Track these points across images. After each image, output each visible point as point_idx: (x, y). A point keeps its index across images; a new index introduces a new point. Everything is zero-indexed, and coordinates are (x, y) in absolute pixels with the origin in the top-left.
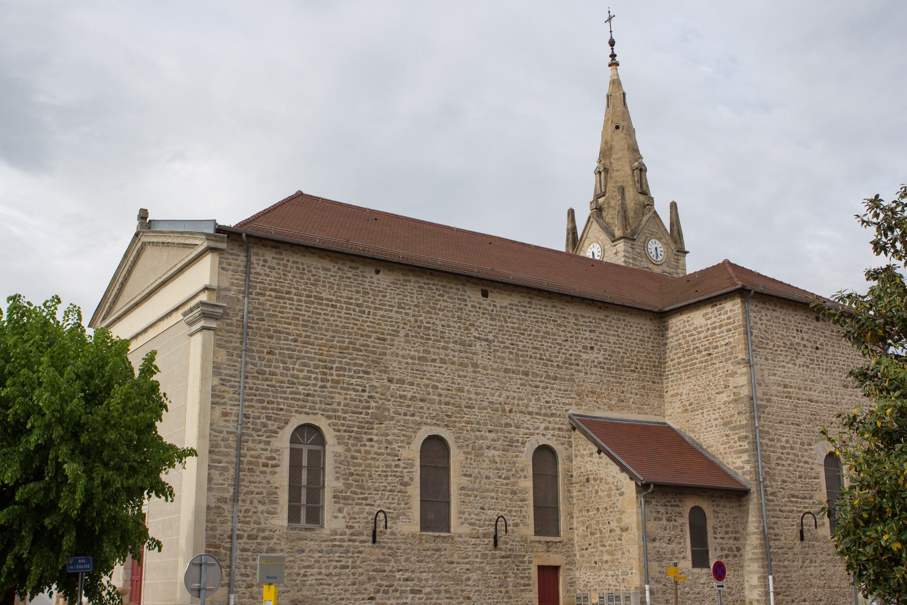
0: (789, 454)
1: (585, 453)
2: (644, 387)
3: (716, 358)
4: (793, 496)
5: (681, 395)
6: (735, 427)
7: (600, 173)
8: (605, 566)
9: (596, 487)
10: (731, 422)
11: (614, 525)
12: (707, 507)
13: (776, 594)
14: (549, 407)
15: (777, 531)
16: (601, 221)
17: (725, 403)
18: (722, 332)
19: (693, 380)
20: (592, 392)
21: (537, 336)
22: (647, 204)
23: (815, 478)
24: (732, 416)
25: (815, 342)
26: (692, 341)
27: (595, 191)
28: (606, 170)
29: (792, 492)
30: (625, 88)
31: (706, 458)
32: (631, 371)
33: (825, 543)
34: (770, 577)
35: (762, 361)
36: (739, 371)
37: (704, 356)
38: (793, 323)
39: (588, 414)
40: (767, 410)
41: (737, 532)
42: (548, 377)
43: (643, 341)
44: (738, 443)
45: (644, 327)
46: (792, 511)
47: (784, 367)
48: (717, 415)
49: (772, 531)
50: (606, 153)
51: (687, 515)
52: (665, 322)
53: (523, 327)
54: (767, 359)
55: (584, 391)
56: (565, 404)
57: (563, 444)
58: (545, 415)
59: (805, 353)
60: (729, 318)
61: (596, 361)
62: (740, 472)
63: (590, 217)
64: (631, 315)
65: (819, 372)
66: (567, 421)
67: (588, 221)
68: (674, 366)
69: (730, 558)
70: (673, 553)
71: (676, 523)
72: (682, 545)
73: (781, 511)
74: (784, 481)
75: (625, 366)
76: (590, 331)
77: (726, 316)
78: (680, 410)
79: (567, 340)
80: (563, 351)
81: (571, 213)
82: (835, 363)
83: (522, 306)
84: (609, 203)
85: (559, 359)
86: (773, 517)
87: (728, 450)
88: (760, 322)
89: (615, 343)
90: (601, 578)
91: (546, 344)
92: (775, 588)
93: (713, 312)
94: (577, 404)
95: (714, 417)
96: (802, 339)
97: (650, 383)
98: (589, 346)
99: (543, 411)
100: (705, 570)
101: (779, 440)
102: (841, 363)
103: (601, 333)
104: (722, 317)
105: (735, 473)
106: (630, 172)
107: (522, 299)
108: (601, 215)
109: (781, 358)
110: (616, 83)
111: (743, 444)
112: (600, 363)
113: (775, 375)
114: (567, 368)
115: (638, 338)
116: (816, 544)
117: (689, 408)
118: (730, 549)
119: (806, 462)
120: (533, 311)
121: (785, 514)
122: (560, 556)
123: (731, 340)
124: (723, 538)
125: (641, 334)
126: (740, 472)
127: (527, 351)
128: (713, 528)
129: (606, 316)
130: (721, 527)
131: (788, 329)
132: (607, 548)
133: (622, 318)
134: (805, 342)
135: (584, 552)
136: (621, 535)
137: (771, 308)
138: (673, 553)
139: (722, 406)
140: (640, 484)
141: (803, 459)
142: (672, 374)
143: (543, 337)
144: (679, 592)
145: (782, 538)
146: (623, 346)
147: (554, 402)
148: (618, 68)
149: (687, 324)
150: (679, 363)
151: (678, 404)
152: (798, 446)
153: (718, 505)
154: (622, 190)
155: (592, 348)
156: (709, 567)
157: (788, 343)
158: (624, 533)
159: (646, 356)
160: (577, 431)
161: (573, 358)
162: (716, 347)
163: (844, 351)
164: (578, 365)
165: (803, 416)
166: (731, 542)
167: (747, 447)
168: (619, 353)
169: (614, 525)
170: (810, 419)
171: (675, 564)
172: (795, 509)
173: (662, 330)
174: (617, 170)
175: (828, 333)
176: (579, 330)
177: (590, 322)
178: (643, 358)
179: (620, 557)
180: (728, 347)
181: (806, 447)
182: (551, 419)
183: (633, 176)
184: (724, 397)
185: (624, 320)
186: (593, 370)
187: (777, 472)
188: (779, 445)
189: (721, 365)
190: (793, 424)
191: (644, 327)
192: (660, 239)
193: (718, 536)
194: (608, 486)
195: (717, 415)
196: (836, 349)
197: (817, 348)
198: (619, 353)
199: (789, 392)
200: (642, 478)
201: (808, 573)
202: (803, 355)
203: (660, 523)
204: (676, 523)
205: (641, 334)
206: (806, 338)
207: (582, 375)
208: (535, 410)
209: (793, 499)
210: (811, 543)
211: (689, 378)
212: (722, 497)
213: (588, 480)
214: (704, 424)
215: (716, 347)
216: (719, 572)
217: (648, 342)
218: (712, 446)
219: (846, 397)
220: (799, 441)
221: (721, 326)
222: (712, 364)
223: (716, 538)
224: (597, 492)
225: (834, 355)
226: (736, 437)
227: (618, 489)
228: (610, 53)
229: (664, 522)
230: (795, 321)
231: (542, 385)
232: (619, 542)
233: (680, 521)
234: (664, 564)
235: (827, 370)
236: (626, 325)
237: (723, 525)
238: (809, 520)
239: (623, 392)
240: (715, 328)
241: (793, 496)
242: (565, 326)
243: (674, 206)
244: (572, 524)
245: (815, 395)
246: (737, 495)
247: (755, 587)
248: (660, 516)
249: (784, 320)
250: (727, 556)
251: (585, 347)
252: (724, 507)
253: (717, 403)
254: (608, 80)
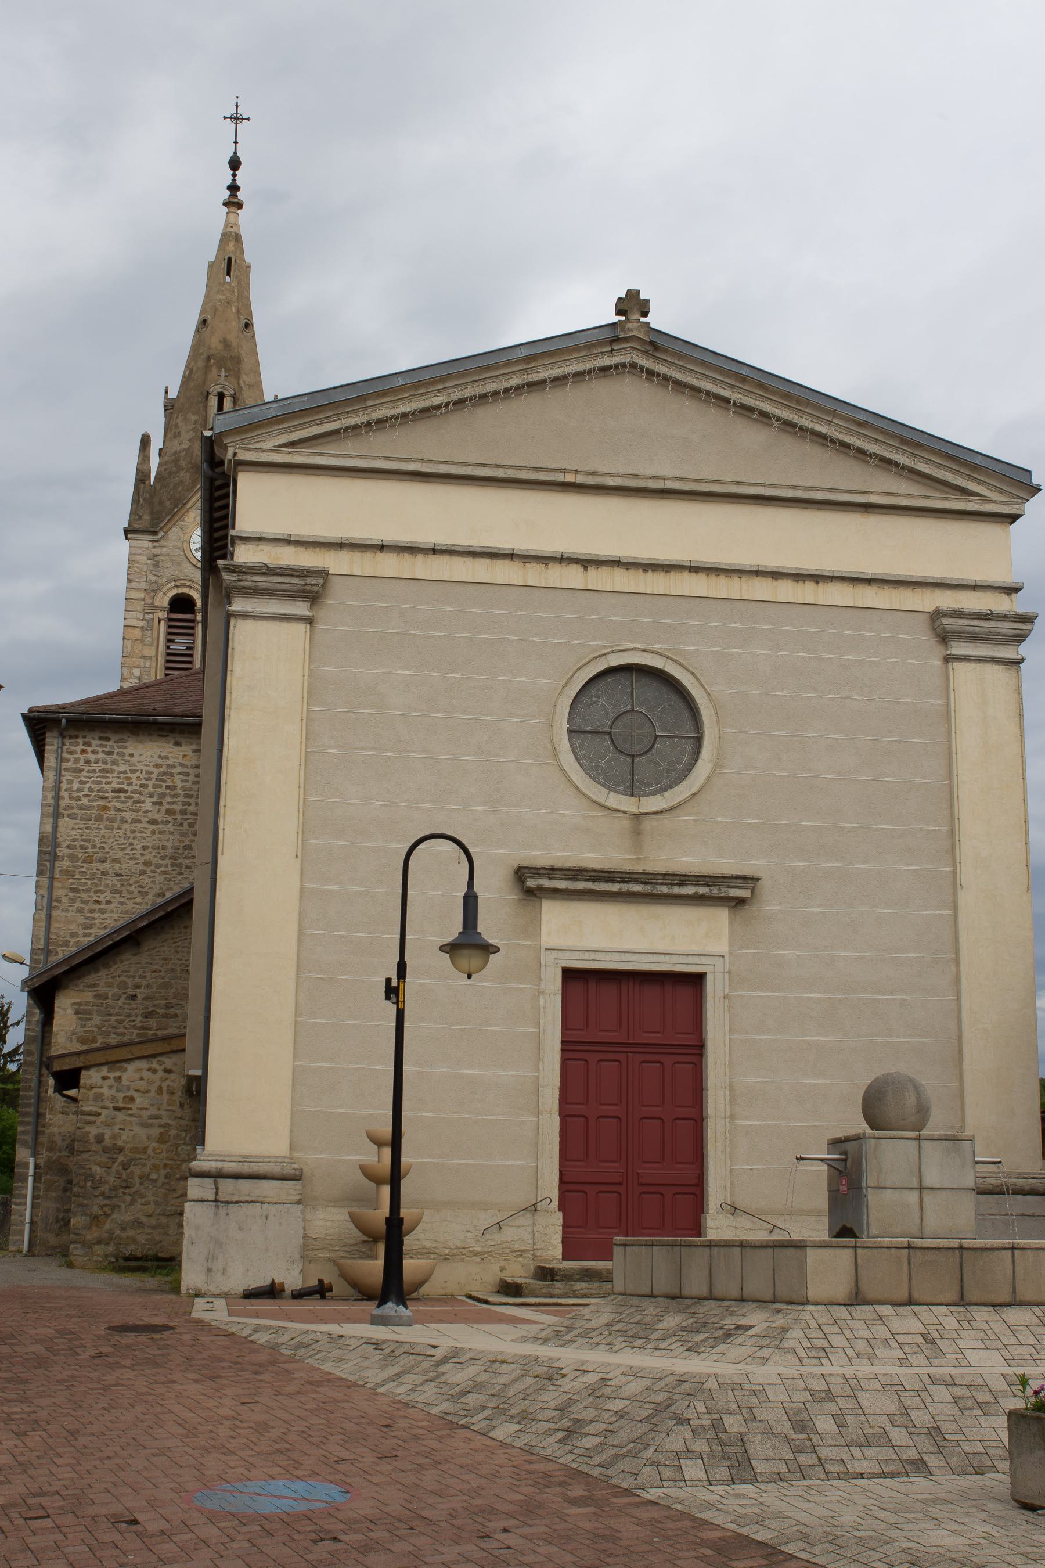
81: (145, 442)
228: (229, 182)
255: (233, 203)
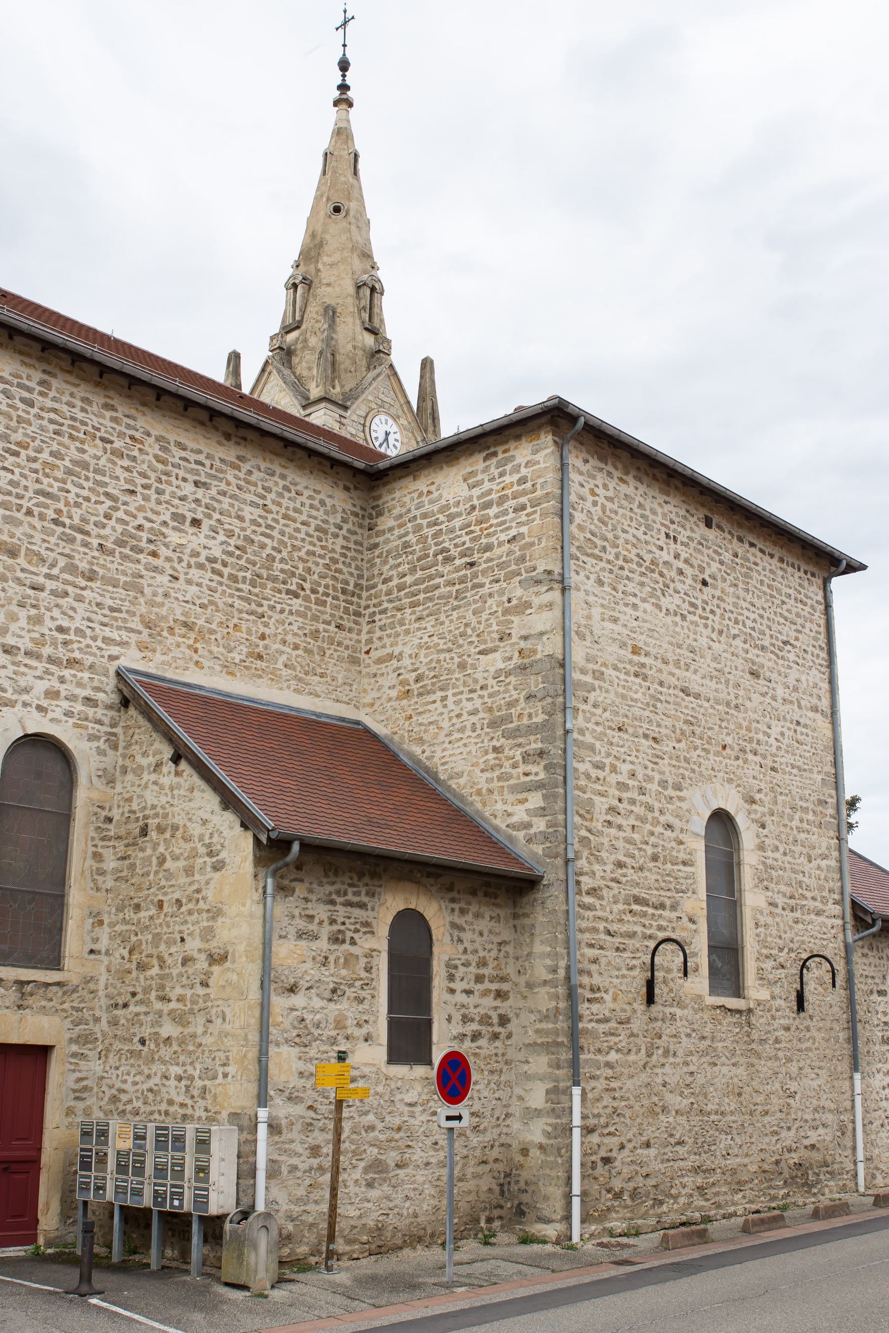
0: (632, 802)
1: (144, 762)
2: (315, 634)
3: (484, 572)
4: (637, 900)
5: (400, 657)
6: (518, 729)
7: (295, 286)
8: (166, 1052)
9: (161, 849)
10: (508, 719)
11: (193, 945)
12: (436, 913)
13: (588, 1131)
14: (65, 643)
15: (596, 980)
16: (287, 372)
17: (498, 673)
18: (505, 513)
19: (429, 623)
20: (185, 624)
21: (53, 467)
22: (378, 354)
23: (684, 863)
24: (511, 704)
25: (702, 570)
26: (435, 535)
27: (283, 321)
28: (308, 282)
29: (636, 891)
30: (359, 145)
31: (444, 802)
32: (288, 592)
33: (696, 1011)
34: (576, 1091)
35: (590, 585)
36: (536, 601)
37: (457, 569)
38: (659, 519)
39: (169, 675)
40: (592, 696)
41: (503, 979)
42: (71, 568)
43: (325, 532)
44: (522, 768)
45: (329, 502)
46: (632, 935)
47: (635, 606)
48: (478, 703)
49: (585, 980)
50: (311, 252)
51: (383, 930)
52: (379, 497)
53: (18, 436)
54: (600, 583)
55: (164, 618)
56: (107, 640)
57: (92, 738)
58: (51, 660)
59: (679, 586)
60: (523, 481)
61: (204, 553)
62: (521, 835)
63: (266, 363)
64: (301, 468)
65: (707, 632)
66: (111, 682)
67: (263, 370)
68: (389, 593)
69: (483, 1042)
70: (340, 1024)
71: (353, 950)
72: (366, 1006)
73: (609, 933)
74: (620, 865)
75: (275, 579)
76: (196, 484)
77: (515, 477)
78: (394, 693)
79: (133, 492)
80: (120, 514)
82: (737, 622)
83: (19, 386)
84: (305, 340)
85: (107, 531)
86: (591, 946)
87: (496, 784)
88: (591, 499)
89: (254, 522)
90: (151, 1084)
91: (74, 490)
92: (584, 1117)
93: (486, 469)
94: (142, 647)
95: (469, 706)
96: (677, 556)
97: (332, 628)
98: (189, 516)
99: (47, 651)
100: (420, 1071)
101: (614, 769)
102: (749, 623)
103: (224, 494)
104: (508, 479)
105: (511, 838)
106: (351, 290)
107: (24, 371)
108: (290, 362)
109: (631, 587)
110: (342, 133)
111: (533, 768)
112: (212, 560)
113: (615, 620)
114: (124, 557)
115: (314, 523)
116: (679, 1012)
117: (415, 687)
118: (485, 1020)
119: (669, 826)
120: (49, 404)
121: (617, 940)
122: (56, 1019)
123: (524, 529)
124: (468, 992)
125: (320, 514)
126: (521, 835)
127: (20, 497)
128: (448, 966)
129: (240, 458)
130: (466, 964)
131: (648, 527)
132: (173, 1005)
133: (279, 470)
134: (681, 565)
135: (119, 1012)
136: (208, 974)
137: (617, 474)
138: (340, 1024)
139: (491, 682)
140: (264, 838)
141: (662, 819)
142: (384, 611)
143: (69, 472)
144: (347, 1126)
145: (608, 998)
146: (275, 533)
147: (79, 632)
148: (352, 111)
149: (425, 499)
150: (401, 588)
151: (392, 679)
152: (654, 787)
153: (463, 912)
154: (331, 313)
155: (196, 523)
156: (430, 1063)
157: (648, 557)
158: (216, 969)
159: (327, 566)
160: (132, 711)
161: (144, 535)
162: (488, 548)
163: (755, 601)
164: (154, 554)
165: (668, 722)
166: (489, 1002)
167: (542, 776)
168: (263, 546)
169: (193, 945)
170: (683, 733)
171: (342, 1057)
172: (638, 929)
173: (369, 516)
174: (328, 285)
175: (727, 557)
176: (167, 474)
177: (197, 462)
178: (320, 569)
179: (200, 1030)
180: (515, 547)
181: (670, 792)
182: (67, 673)
183: (358, 297)
184: (496, 661)
185: (283, 477)
186: (195, 574)
187: (605, 840)
188: (613, 779)
189: (496, 587)
190: (646, 736)
191: (329, 502)
192: (395, 418)
193: (458, 986)
194: (188, 846)
195: (478, 703)
196: (742, 593)
197: (704, 583)
198: (263, 546)
199: (643, 665)
200: (271, 824)
201: (659, 1080)
202: (677, 592)
203: (315, 945)
204: (353, 950)
205: (320, 514)
206: (684, 555)
207: (164, 579)
208: (25, 644)
209: (635, 907)
210: (668, 1010)
211: (420, 619)
212: (474, 893)
213: (144, 832)
214: (446, 724)
215: (488, 548)
216: (454, 1080)
217: (336, 536)
218: (460, 775)
219: (754, 696)
220: (657, 777)
221: (502, 500)
222: (475, 586)
223: (452, 991)
224: (162, 860)
225: (735, 605)
226: (518, 754)
227: (210, 854)
229: (323, 944)
230: (664, 515)
231: (50, 585)
232: (201, 991)
233: (366, 943)
234: (313, 1052)
235: (721, 632)
236: (287, 489)
237: (473, 959)
238: (669, 958)
239: (263, 637)
240: (488, 505)
241: (637, 900)
242: (134, 459)
243: (427, 366)
244: (96, 940)
245: (694, 682)
246: (507, 887)
247: (538, 1113)
248: (313, 927)
249: (640, 506)
250: (476, 1036)
251: (178, 518)
252: (477, 916)
253: (479, 676)
254: (330, 128)
255: (343, 100)
